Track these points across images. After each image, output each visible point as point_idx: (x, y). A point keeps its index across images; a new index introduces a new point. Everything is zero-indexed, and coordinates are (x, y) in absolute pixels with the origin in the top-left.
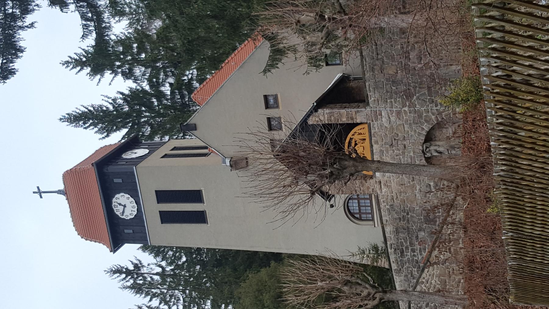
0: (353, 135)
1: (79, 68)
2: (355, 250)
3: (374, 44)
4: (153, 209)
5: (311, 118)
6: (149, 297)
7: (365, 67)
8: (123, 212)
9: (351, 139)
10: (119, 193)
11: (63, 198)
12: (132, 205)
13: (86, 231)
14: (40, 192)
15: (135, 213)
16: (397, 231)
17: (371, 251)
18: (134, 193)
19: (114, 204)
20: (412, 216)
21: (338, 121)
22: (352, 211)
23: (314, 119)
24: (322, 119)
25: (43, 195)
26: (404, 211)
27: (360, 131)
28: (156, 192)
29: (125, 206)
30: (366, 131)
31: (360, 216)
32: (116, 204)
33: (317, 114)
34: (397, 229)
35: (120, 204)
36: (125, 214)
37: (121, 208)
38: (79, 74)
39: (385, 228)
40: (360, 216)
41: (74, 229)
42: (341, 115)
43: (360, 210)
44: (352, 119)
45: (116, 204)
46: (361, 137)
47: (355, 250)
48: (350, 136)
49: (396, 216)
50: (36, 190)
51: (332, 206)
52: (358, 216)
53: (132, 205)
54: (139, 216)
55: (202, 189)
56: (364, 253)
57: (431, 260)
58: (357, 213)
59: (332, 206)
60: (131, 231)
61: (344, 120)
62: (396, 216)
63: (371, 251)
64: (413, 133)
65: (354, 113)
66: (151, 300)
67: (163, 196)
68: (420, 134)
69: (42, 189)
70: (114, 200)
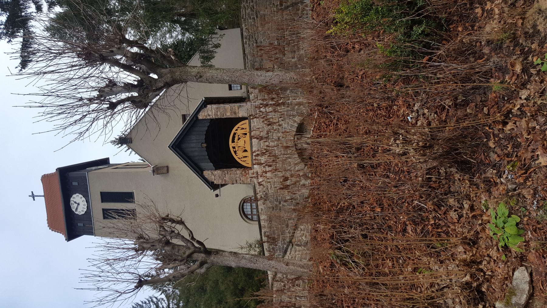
0: (237, 130)
1: (120, 145)
2: (244, 244)
3: (255, 41)
4: (98, 206)
5: (201, 113)
6: (161, 292)
7: (247, 65)
8: (77, 209)
9: (235, 134)
10: (75, 194)
11: (43, 198)
12: (84, 203)
13: (53, 225)
14: (33, 196)
15: (85, 210)
16: (270, 220)
17: (257, 245)
18: (86, 195)
19: (71, 202)
20: (284, 206)
21: (223, 115)
22: (246, 213)
23: (203, 114)
24: (210, 113)
25: (35, 198)
26: (277, 200)
27: (242, 127)
28: (101, 193)
29: (78, 204)
30: (246, 126)
31: (252, 217)
32: (73, 202)
33: (205, 109)
34: (270, 218)
35: (75, 202)
36: (78, 210)
37: (76, 205)
38: (131, 155)
39: (261, 217)
40: (252, 217)
41: (46, 222)
42: (225, 110)
43: (252, 211)
44: (235, 113)
45: (73, 202)
46: (243, 131)
47: (244, 244)
48: (234, 131)
49: (270, 205)
50: (31, 194)
51: (217, 196)
52: (250, 217)
53: (84, 203)
54: (88, 212)
55: (134, 191)
56: (251, 246)
57: (293, 240)
58: (249, 215)
59: (217, 196)
60: (82, 225)
61: (228, 115)
62: (270, 205)
63: (257, 245)
64: (286, 126)
65: (237, 108)
66: (161, 294)
67: (106, 197)
68: (292, 126)
69: (35, 194)
70: (72, 199)
